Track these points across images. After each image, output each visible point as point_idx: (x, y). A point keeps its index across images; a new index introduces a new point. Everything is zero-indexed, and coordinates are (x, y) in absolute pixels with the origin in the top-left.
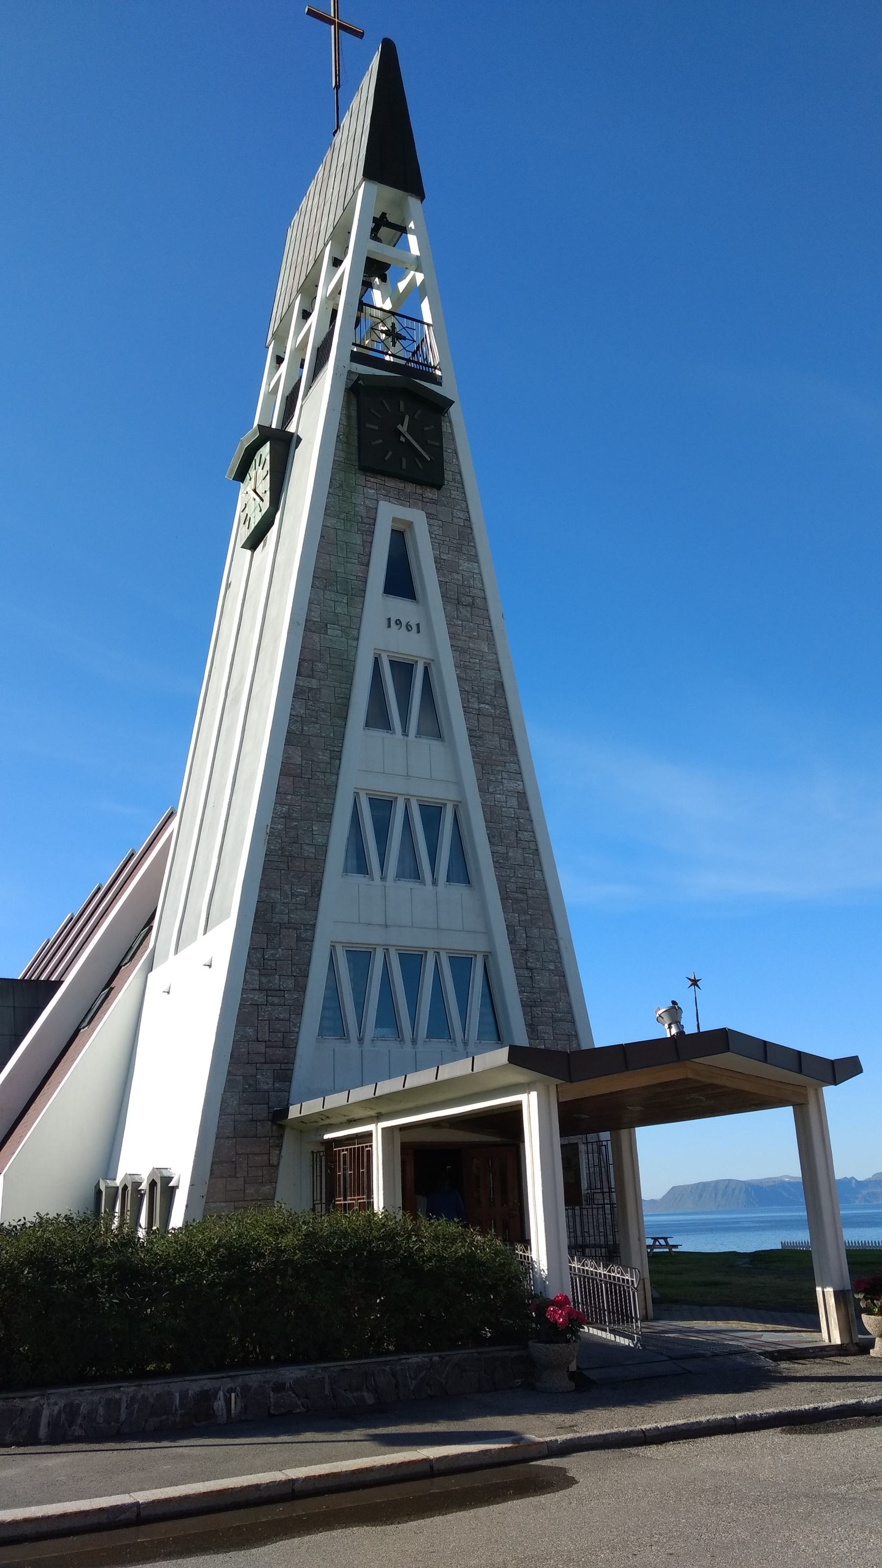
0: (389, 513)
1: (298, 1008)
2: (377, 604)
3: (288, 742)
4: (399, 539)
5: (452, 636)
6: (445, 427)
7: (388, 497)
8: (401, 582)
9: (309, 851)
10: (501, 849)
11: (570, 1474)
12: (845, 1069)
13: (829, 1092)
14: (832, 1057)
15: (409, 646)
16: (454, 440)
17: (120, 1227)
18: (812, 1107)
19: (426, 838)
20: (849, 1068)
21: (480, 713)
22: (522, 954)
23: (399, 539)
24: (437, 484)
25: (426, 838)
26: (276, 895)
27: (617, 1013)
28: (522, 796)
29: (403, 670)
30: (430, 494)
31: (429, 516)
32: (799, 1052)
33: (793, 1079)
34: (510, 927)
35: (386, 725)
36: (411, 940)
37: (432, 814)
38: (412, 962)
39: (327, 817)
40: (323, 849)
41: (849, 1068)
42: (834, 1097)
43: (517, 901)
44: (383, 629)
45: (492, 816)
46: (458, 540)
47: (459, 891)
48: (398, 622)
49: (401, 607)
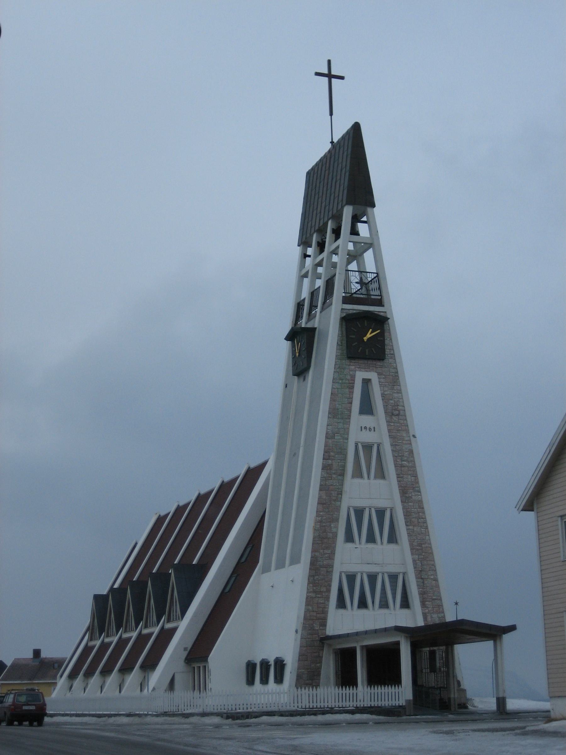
0: (360, 375)
1: (328, 598)
2: (357, 420)
3: (320, 490)
4: (366, 382)
5: (389, 431)
7: (360, 368)
8: (367, 408)
9: (330, 535)
15: (368, 437)
19: (374, 525)
21: (402, 466)
22: (420, 574)
23: (366, 382)
25: (374, 525)
26: (329, 482)
28: (420, 502)
29: (368, 447)
30: (379, 363)
31: (379, 374)
34: (414, 561)
35: (361, 476)
37: (381, 513)
38: (372, 578)
39: (337, 520)
40: (335, 535)
41: (512, 628)
42: (507, 638)
44: (365, 429)
45: (407, 514)
46: (393, 381)
47: (392, 546)
48: (365, 428)
49: (367, 420)
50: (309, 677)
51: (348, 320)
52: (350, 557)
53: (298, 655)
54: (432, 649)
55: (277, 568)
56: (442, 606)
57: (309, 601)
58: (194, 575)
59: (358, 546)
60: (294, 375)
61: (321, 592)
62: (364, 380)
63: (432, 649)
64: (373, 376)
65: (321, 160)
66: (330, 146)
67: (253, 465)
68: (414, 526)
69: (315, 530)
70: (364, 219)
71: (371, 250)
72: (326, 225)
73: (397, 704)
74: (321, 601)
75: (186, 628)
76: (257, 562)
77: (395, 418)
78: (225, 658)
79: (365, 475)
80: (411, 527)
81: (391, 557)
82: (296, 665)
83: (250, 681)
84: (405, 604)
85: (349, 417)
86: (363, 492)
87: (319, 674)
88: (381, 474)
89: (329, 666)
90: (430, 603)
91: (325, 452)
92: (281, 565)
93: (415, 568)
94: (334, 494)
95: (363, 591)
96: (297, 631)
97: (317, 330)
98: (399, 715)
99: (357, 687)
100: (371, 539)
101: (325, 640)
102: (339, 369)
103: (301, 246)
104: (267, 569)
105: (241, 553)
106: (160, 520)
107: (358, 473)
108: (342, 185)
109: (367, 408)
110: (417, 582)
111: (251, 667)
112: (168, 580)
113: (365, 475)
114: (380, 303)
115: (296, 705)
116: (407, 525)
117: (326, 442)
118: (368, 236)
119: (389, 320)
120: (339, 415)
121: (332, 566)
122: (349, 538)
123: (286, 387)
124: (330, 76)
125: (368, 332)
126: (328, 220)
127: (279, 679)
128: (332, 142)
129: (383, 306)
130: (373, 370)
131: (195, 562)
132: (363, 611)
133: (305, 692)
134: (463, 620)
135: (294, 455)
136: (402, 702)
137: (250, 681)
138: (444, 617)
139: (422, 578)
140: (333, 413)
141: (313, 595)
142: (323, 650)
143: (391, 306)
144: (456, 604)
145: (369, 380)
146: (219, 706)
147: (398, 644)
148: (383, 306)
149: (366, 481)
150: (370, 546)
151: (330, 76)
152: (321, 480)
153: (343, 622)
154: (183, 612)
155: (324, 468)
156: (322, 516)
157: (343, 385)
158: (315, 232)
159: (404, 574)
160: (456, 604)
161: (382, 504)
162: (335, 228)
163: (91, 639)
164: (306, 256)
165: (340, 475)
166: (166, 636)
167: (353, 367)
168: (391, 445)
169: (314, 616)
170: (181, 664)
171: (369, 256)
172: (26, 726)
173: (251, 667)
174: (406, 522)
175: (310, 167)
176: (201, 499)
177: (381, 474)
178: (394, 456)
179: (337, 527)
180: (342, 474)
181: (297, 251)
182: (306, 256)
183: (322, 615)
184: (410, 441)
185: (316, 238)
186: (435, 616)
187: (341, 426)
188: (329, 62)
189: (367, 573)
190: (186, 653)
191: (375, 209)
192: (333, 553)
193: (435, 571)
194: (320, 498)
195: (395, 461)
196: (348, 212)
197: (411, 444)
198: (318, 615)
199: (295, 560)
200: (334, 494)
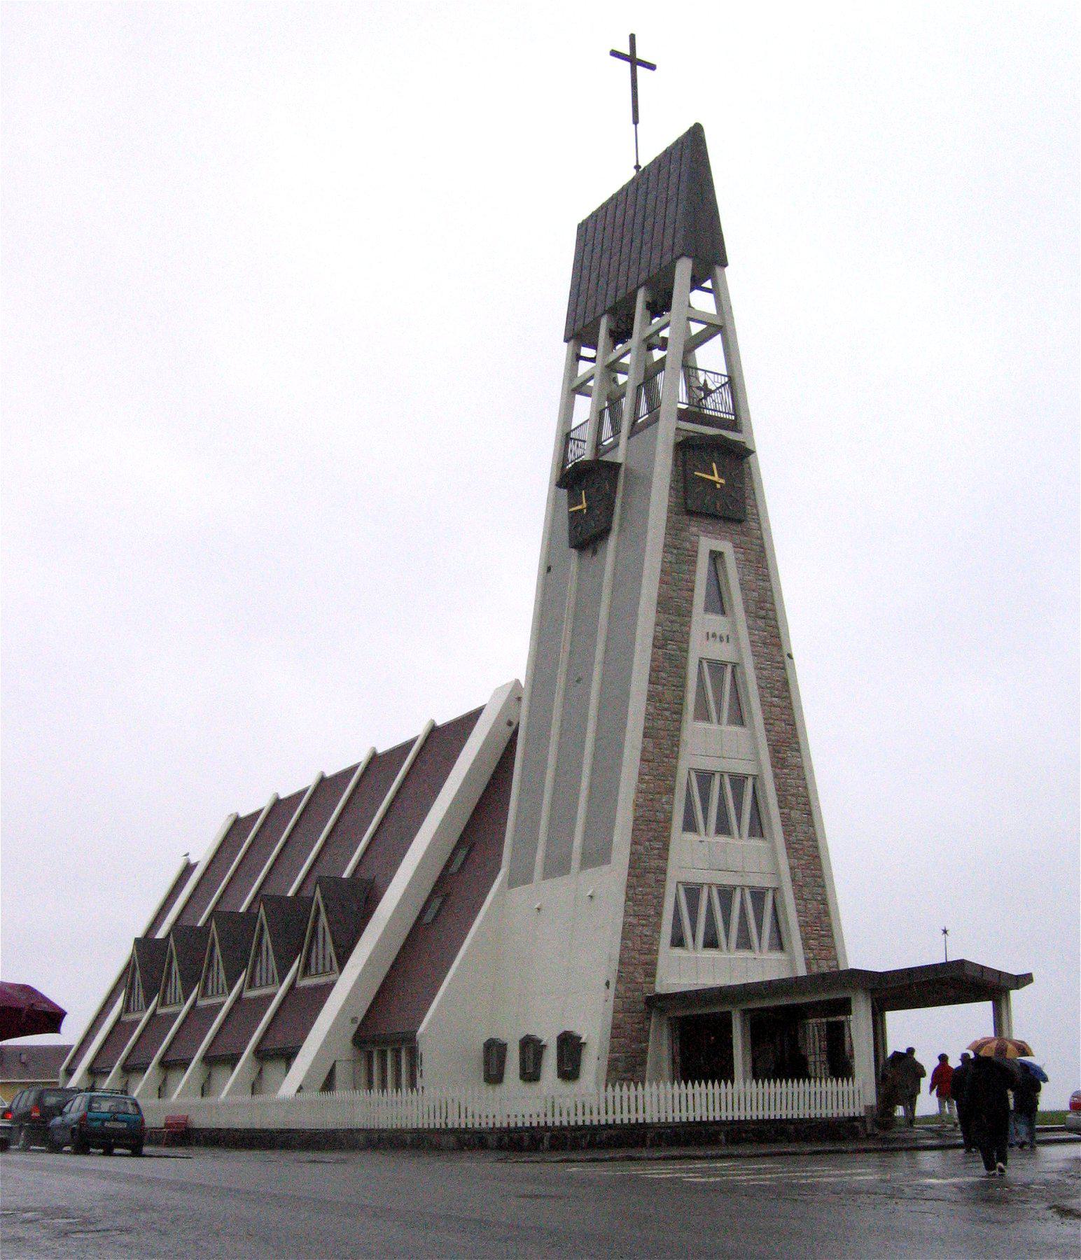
0: (707, 544)
1: (657, 927)
2: (702, 622)
4: (716, 557)
6: (746, 471)
8: (718, 603)
9: (660, 816)
10: (786, 811)
11: (582, 1041)
12: (1023, 980)
13: (1013, 993)
14: (1016, 974)
15: (721, 652)
16: (616, 1027)
17: (383, 1055)
18: (1004, 1005)
20: (1026, 979)
21: (772, 705)
23: (716, 557)
24: (740, 521)
27: (870, 945)
29: (717, 667)
32: (983, 967)
33: (987, 986)
34: (791, 868)
35: (707, 718)
36: (727, 880)
37: (738, 781)
38: (726, 894)
39: (671, 790)
40: (669, 820)
41: (1026, 979)
42: (1014, 994)
43: (796, 850)
46: (758, 560)
47: (756, 842)
48: (714, 635)
49: (716, 623)
50: (627, 1067)
51: (686, 448)
52: (694, 857)
53: (609, 1028)
54: (831, 1019)
55: (547, 875)
56: (834, 947)
57: (627, 932)
58: (357, 901)
59: (703, 837)
60: (575, 547)
61: (646, 917)
62: (712, 552)
63: (831, 1019)
64: (726, 547)
65: (594, 216)
66: (634, 172)
67: (329, 773)
68: (792, 809)
69: (637, 806)
70: (708, 284)
71: (718, 337)
72: (633, 297)
73: (512, 1125)
74: (647, 931)
75: (349, 986)
76: (497, 869)
77: (761, 623)
78: (450, 1021)
79: (714, 715)
80: (786, 811)
81: (751, 860)
82: (607, 1044)
83: (494, 1075)
84: (779, 943)
85: (689, 613)
86: (711, 744)
87: (644, 1063)
88: (739, 718)
89: (660, 1047)
90: (816, 943)
91: (653, 670)
92: (558, 867)
93: (793, 880)
94: (666, 743)
95: (720, 914)
96: (608, 984)
97: (623, 469)
98: (841, 1139)
99: (732, 1083)
100: (723, 828)
101: (658, 1003)
102: (674, 530)
103: (572, 342)
104: (521, 878)
105: (446, 857)
106: (239, 826)
107: (703, 714)
108: (653, 246)
109: (718, 603)
110: (797, 905)
111: (494, 1052)
112: (269, 912)
113: (714, 715)
114: (735, 425)
115: (426, 1121)
116: (780, 807)
117: (653, 653)
118: (714, 312)
119: (751, 458)
120: (674, 609)
121: (664, 872)
122: (690, 826)
123: (549, 569)
124: (633, 60)
125: (717, 471)
126: (638, 288)
127: (569, 1071)
128: (637, 167)
129: (740, 431)
130: (724, 538)
131: (346, 874)
132: (711, 953)
133: (627, 1092)
134: (961, 963)
135: (578, 680)
136: (858, 1111)
137: (494, 1075)
138: (838, 966)
139: (803, 899)
140: (664, 604)
141: (634, 921)
142: (649, 1019)
143: (751, 433)
144: (945, 932)
145: (721, 554)
146: (534, 1116)
147: (730, 1013)
148: (740, 431)
149: (714, 726)
150: (722, 839)
151: (633, 60)
152: (647, 720)
153: (685, 970)
154: (342, 960)
155: (651, 697)
156: (647, 782)
157: (679, 556)
158: (605, 312)
159: (775, 890)
160: (945, 932)
161: (742, 768)
162: (649, 299)
163: (127, 1009)
164: (579, 357)
165: (675, 713)
166: (305, 1004)
167: (694, 529)
168: (756, 668)
169: (637, 958)
170: (345, 1047)
171: (710, 357)
172: (67, 1152)
173: (494, 1052)
174: (779, 801)
175: (585, 214)
176: (280, 807)
177: (739, 718)
178: (760, 687)
179: (671, 803)
180: (679, 713)
181: (562, 350)
182: (579, 357)
183: (648, 957)
184: (783, 663)
185: (645, 296)
186: (823, 963)
187: (676, 627)
188: (632, 37)
189: (718, 886)
190: (356, 1026)
191: (726, 269)
192: (666, 847)
193: (824, 887)
194: (644, 750)
195: (762, 697)
196: (684, 269)
197: (784, 668)
198: (643, 957)
199: (597, 856)
200: (666, 743)
